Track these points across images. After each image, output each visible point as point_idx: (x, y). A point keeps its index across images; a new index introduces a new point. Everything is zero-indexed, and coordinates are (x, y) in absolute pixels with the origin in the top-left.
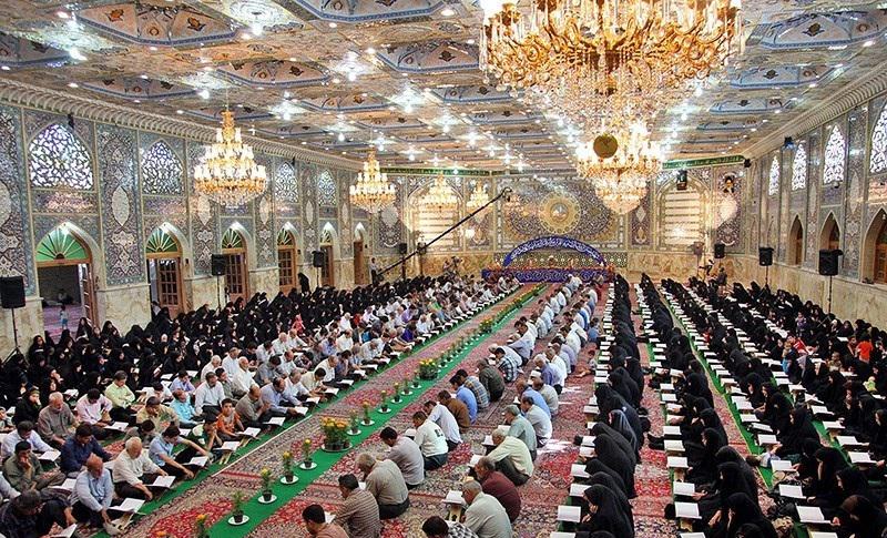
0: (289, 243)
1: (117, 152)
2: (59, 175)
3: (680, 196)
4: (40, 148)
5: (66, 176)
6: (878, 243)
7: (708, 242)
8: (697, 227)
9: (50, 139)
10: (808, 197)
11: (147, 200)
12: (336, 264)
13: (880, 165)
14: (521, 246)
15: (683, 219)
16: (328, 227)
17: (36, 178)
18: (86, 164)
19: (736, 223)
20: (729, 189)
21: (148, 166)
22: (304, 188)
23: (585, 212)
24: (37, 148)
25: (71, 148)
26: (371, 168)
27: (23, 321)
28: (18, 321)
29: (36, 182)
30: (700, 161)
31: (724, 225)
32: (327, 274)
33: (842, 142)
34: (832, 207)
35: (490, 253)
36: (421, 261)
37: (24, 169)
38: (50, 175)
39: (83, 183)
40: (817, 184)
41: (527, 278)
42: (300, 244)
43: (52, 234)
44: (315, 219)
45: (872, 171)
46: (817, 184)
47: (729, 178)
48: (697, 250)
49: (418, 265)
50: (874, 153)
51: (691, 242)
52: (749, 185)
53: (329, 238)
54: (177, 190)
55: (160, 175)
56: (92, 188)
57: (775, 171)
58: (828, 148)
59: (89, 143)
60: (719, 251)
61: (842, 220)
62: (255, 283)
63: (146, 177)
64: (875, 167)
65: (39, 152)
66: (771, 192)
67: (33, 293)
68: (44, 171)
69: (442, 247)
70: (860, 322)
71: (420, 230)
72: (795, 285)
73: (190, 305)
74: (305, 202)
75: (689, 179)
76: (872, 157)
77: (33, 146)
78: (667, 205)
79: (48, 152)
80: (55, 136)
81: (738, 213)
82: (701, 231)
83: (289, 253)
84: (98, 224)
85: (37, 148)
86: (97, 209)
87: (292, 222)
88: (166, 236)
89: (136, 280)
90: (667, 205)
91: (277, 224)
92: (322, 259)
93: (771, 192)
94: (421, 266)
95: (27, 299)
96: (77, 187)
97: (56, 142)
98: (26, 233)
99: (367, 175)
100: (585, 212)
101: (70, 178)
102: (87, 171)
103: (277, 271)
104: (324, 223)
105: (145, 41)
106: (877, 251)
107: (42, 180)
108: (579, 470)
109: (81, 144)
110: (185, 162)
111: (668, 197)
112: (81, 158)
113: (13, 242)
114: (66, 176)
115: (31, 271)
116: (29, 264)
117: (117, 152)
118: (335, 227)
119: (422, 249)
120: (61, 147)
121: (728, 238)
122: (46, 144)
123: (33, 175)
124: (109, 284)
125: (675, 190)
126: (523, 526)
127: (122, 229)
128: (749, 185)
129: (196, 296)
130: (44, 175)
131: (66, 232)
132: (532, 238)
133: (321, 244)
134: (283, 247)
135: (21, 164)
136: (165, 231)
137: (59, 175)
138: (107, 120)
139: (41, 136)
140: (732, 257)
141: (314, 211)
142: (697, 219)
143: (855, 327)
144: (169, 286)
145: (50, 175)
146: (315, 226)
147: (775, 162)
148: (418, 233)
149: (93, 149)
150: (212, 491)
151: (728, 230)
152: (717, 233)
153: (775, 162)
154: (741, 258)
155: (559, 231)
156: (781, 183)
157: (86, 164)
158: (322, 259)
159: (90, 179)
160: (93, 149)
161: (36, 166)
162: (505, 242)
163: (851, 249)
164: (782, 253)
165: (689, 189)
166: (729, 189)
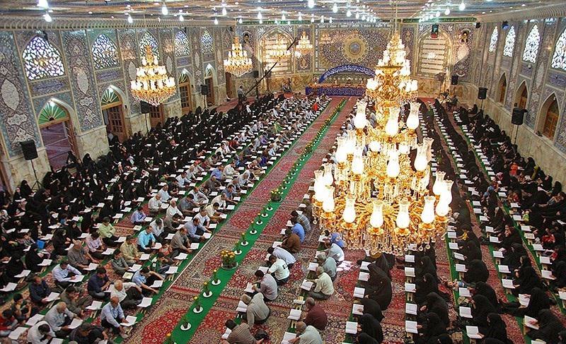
0: (186, 81)
1: (76, 47)
2: (43, 70)
3: (433, 42)
4: (29, 55)
5: (48, 69)
6: (549, 110)
7: (448, 72)
8: (442, 62)
9: (34, 48)
10: (513, 65)
11: (98, 74)
12: (215, 89)
13: (558, 64)
14: (330, 71)
15: (434, 47)
16: (209, 66)
17: (30, 75)
18: (58, 59)
19: (467, 61)
20: (465, 40)
21: (96, 52)
22: (193, 44)
23: (371, 49)
24: (27, 55)
25: (48, 51)
26: (237, 48)
27: (38, 163)
28: (35, 164)
29: (30, 78)
30: (448, 19)
31: (459, 63)
32: (211, 101)
33: (538, 37)
34: (526, 78)
35: (311, 74)
36: (267, 81)
37: (22, 71)
38: (38, 71)
39: (57, 72)
40: (519, 58)
41: (332, 92)
42: (192, 81)
43: (45, 107)
44: (201, 64)
45: (553, 66)
46: (519, 58)
47: (465, 32)
48: (441, 78)
49: (266, 84)
50: (556, 55)
51: (438, 72)
52: (478, 38)
53: (210, 73)
54: (115, 63)
55: (104, 56)
56: (64, 74)
57: (494, 36)
58: (529, 37)
59: (57, 45)
60: (455, 80)
61: (531, 86)
62: (167, 112)
63: (96, 59)
64: (555, 64)
65: (29, 58)
66: (491, 50)
67: (40, 146)
68: (34, 69)
69: (280, 71)
70: (531, 159)
71: (267, 61)
72: (497, 116)
73: (130, 133)
74: (194, 54)
75: (439, 31)
76: (554, 56)
77: (24, 55)
78: (423, 66)
79: (34, 57)
80: (37, 44)
81: (469, 56)
82: (445, 65)
83: (186, 87)
84: (71, 95)
85: (27, 55)
86: (69, 87)
87: (187, 68)
88: (111, 94)
89: (98, 125)
90: (423, 66)
91: (177, 72)
92: (207, 89)
93: (491, 50)
94: (268, 85)
95: (37, 150)
96: (55, 75)
97: (38, 48)
98: (30, 111)
99: (234, 53)
100: (371, 49)
101: (51, 70)
102: (59, 63)
103: (180, 102)
104: (206, 65)
105: (91, 5)
106: (548, 115)
107: (34, 75)
108: (359, 292)
109: (53, 47)
110: (118, 45)
111: (425, 41)
112: (55, 56)
113: (24, 118)
114: (48, 69)
115: (37, 133)
116: (35, 129)
117: (76, 47)
118: (213, 65)
119: (268, 74)
120: (41, 51)
121: (461, 72)
122: (32, 51)
123: (28, 73)
124: (83, 131)
125: (430, 37)
126: (328, 330)
127: (86, 96)
128: (478, 38)
129: (133, 127)
130: (35, 72)
131: (53, 105)
132: (337, 65)
133: (205, 78)
134: (182, 85)
135: (20, 68)
136: (111, 91)
137: (43, 70)
138: (67, 28)
139: (28, 47)
140: (462, 84)
141: (200, 59)
142: (442, 57)
143: (527, 161)
144: (116, 121)
145: (38, 71)
146: (202, 68)
147: (496, 31)
148: (266, 63)
149: (61, 49)
150: (168, 303)
151: (461, 67)
152: (454, 68)
153: (496, 31)
154: (468, 85)
155: (355, 60)
156: (497, 45)
157: (58, 59)
158: (207, 89)
159: (62, 69)
160: (61, 49)
161: (29, 67)
162: (319, 67)
163: (533, 110)
164: (492, 93)
165: (440, 38)
166: (465, 40)
